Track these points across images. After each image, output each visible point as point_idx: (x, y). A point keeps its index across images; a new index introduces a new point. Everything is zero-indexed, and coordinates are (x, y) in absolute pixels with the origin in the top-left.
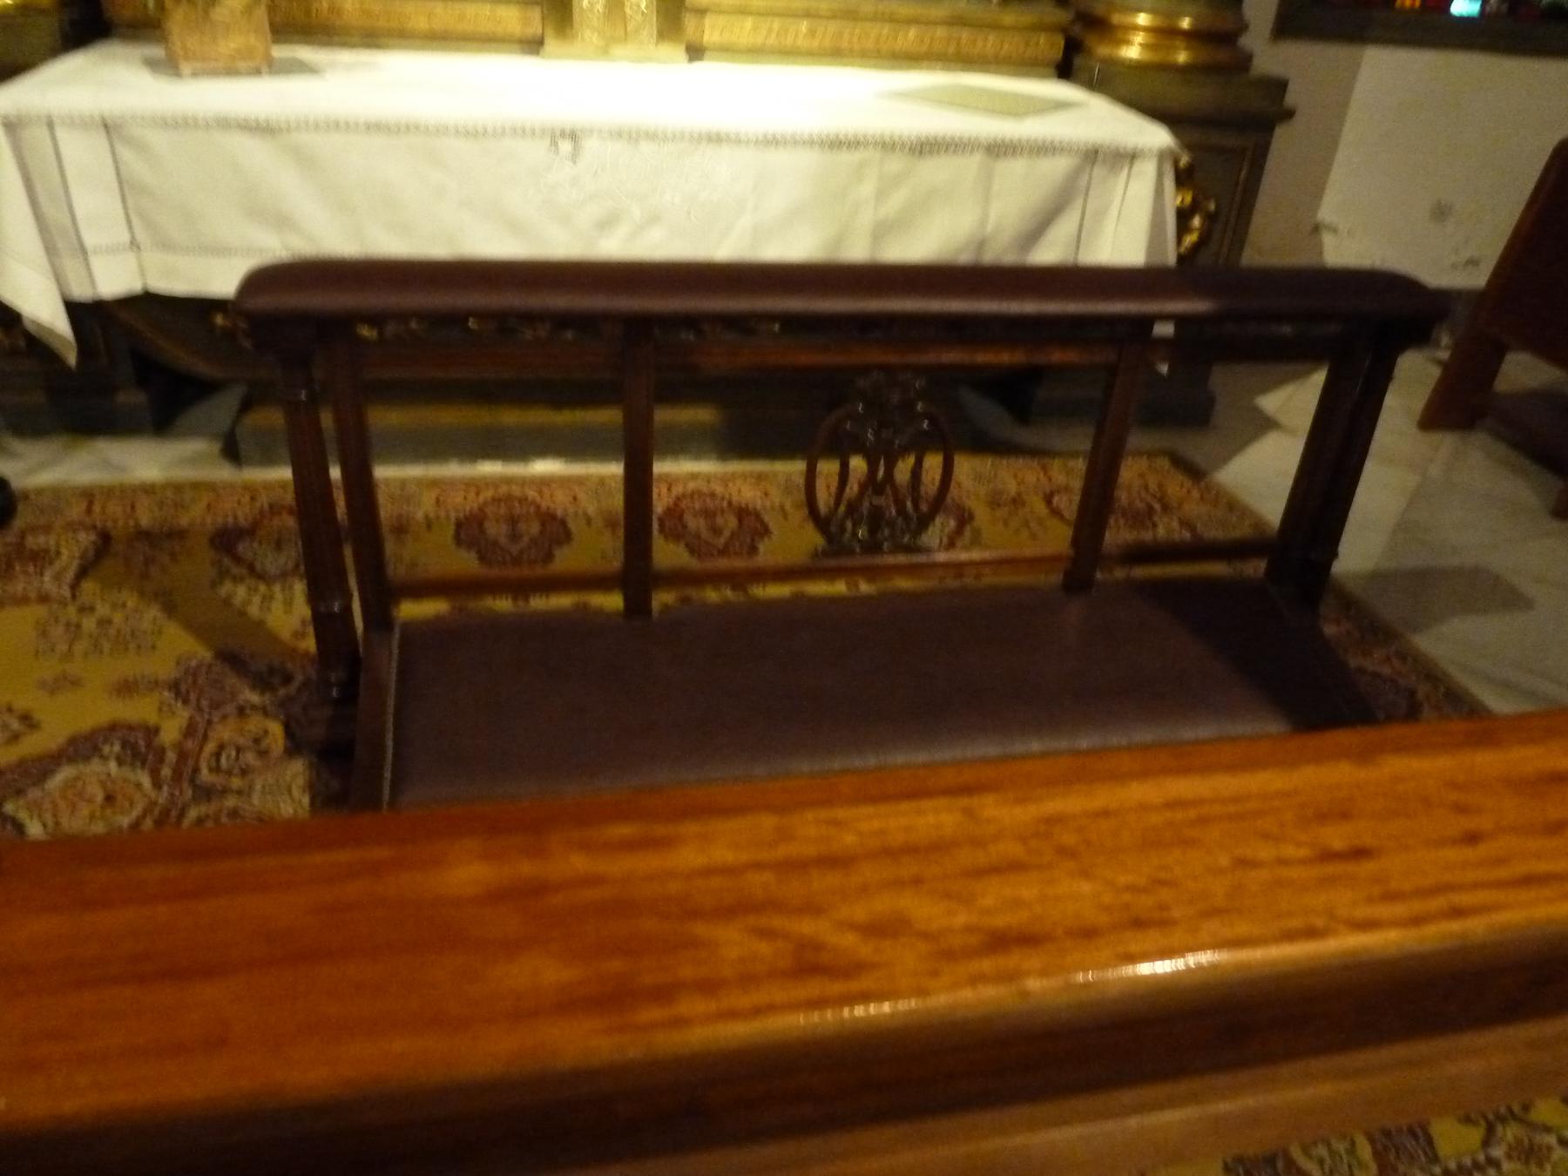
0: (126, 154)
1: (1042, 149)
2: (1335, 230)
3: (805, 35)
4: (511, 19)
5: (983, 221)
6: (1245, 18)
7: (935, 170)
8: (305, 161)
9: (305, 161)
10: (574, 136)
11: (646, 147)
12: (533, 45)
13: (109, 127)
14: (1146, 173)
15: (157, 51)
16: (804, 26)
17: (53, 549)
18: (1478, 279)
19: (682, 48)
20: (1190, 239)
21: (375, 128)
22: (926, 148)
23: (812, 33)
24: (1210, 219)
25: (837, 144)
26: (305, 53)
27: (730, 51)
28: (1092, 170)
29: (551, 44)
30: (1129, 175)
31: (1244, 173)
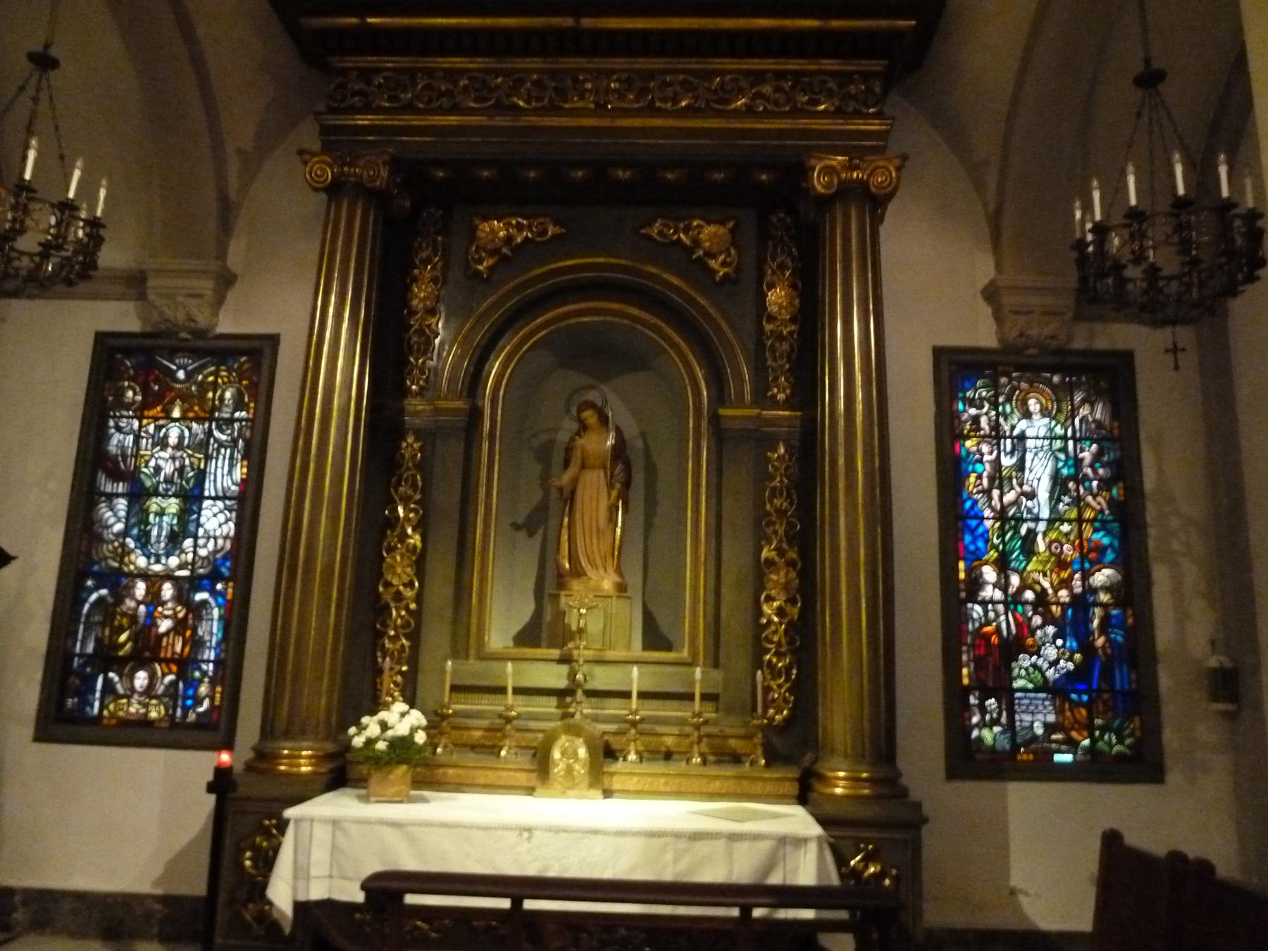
0: (338, 834)
1: (756, 837)
2: (1026, 894)
4: (522, 778)
5: (731, 872)
7: (702, 848)
8: (412, 839)
9: (412, 839)
10: (529, 830)
11: (562, 835)
12: (530, 791)
13: (335, 823)
14: (813, 847)
15: (363, 792)
16: (662, 781)
19: (601, 792)
21: (444, 825)
22: (697, 836)
23: (666, 784)
25: (651, 834)
26: (426, 793)
27: (626, 793)
28: (784, 849)
29: (539, 790)
30: (805, 850)
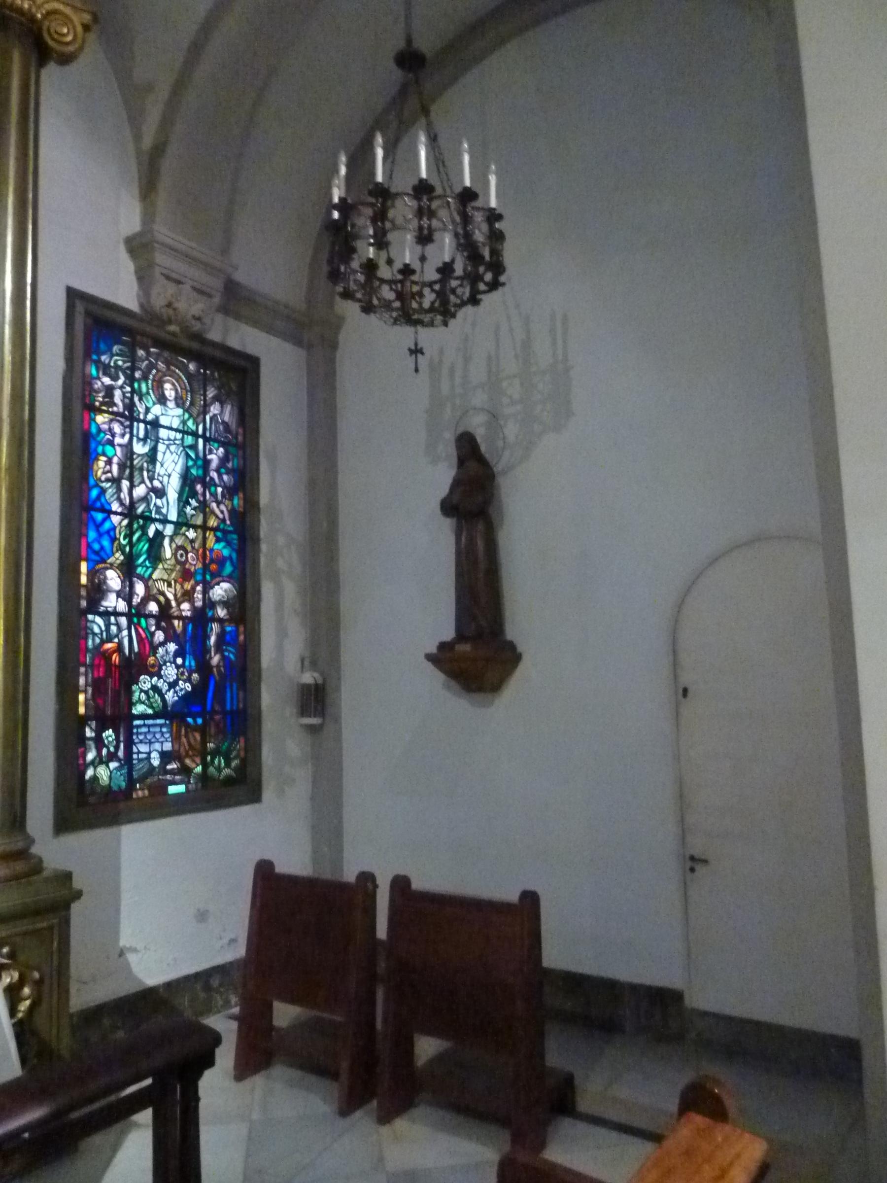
2: (134, 950)
3: (151, 430)
6: (21, 1004)
17: (434, 194)
18: (240, 951)
20: (24, 1006)
24: (38, 985)
31: (55, 944)
